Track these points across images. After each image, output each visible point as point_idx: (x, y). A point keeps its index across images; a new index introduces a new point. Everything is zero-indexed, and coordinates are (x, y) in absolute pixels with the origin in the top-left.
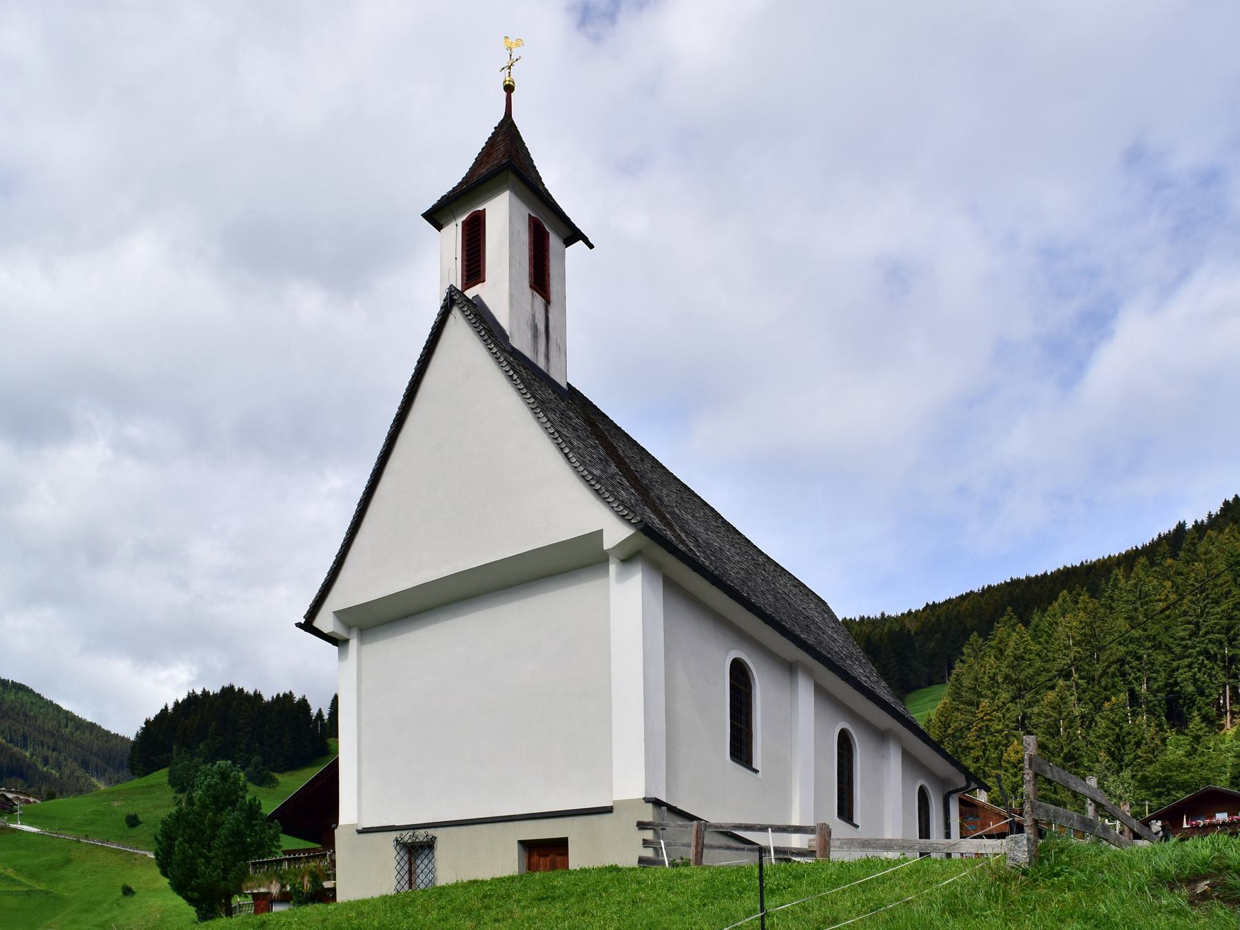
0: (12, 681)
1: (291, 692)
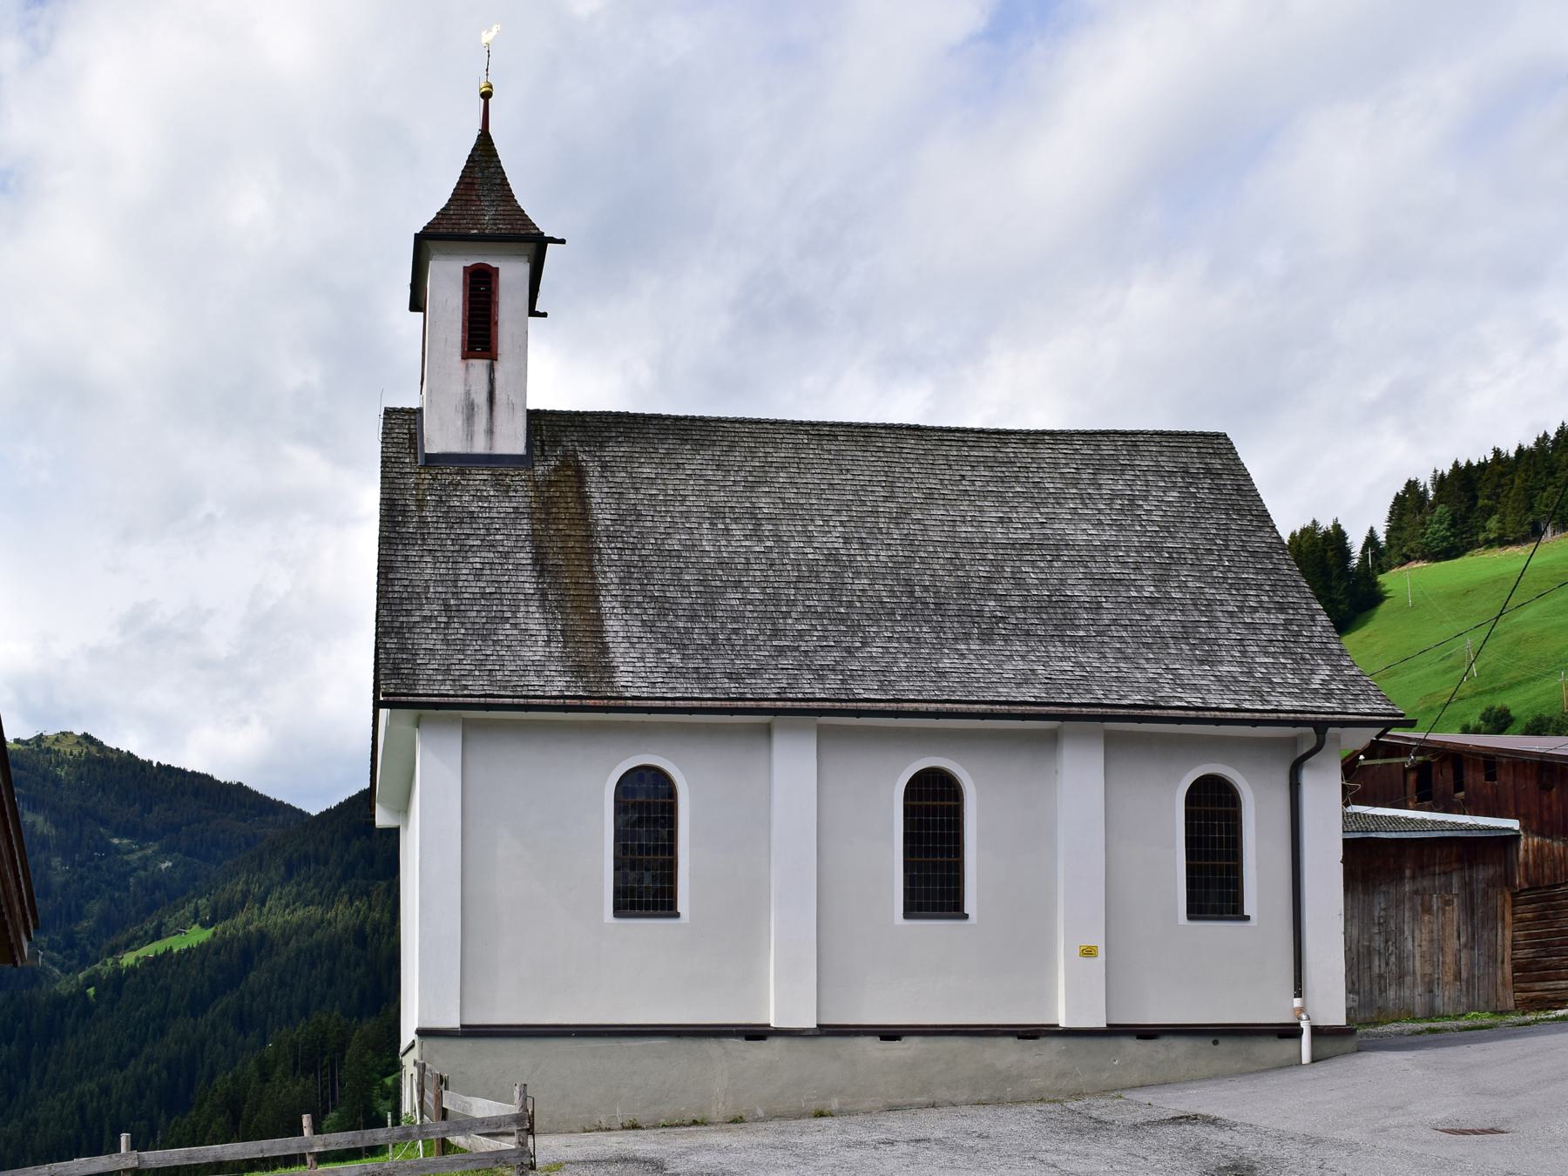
0: (158, 763)
1: (1314, 522)
